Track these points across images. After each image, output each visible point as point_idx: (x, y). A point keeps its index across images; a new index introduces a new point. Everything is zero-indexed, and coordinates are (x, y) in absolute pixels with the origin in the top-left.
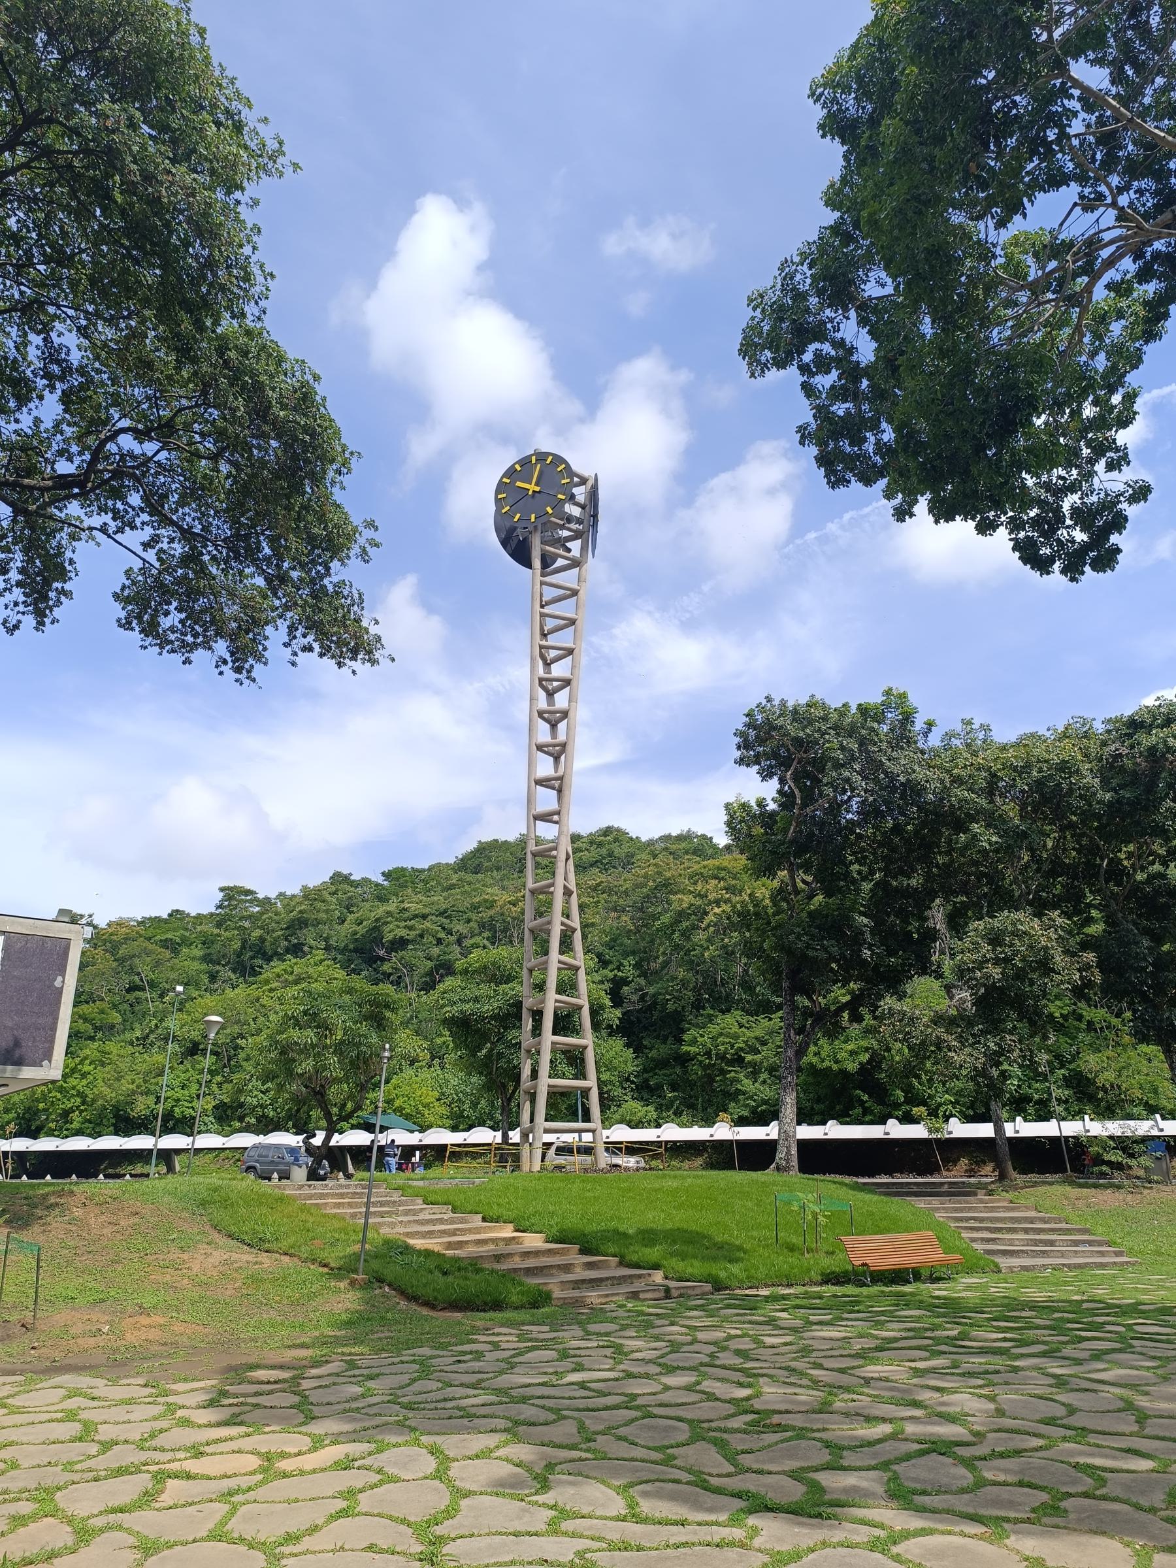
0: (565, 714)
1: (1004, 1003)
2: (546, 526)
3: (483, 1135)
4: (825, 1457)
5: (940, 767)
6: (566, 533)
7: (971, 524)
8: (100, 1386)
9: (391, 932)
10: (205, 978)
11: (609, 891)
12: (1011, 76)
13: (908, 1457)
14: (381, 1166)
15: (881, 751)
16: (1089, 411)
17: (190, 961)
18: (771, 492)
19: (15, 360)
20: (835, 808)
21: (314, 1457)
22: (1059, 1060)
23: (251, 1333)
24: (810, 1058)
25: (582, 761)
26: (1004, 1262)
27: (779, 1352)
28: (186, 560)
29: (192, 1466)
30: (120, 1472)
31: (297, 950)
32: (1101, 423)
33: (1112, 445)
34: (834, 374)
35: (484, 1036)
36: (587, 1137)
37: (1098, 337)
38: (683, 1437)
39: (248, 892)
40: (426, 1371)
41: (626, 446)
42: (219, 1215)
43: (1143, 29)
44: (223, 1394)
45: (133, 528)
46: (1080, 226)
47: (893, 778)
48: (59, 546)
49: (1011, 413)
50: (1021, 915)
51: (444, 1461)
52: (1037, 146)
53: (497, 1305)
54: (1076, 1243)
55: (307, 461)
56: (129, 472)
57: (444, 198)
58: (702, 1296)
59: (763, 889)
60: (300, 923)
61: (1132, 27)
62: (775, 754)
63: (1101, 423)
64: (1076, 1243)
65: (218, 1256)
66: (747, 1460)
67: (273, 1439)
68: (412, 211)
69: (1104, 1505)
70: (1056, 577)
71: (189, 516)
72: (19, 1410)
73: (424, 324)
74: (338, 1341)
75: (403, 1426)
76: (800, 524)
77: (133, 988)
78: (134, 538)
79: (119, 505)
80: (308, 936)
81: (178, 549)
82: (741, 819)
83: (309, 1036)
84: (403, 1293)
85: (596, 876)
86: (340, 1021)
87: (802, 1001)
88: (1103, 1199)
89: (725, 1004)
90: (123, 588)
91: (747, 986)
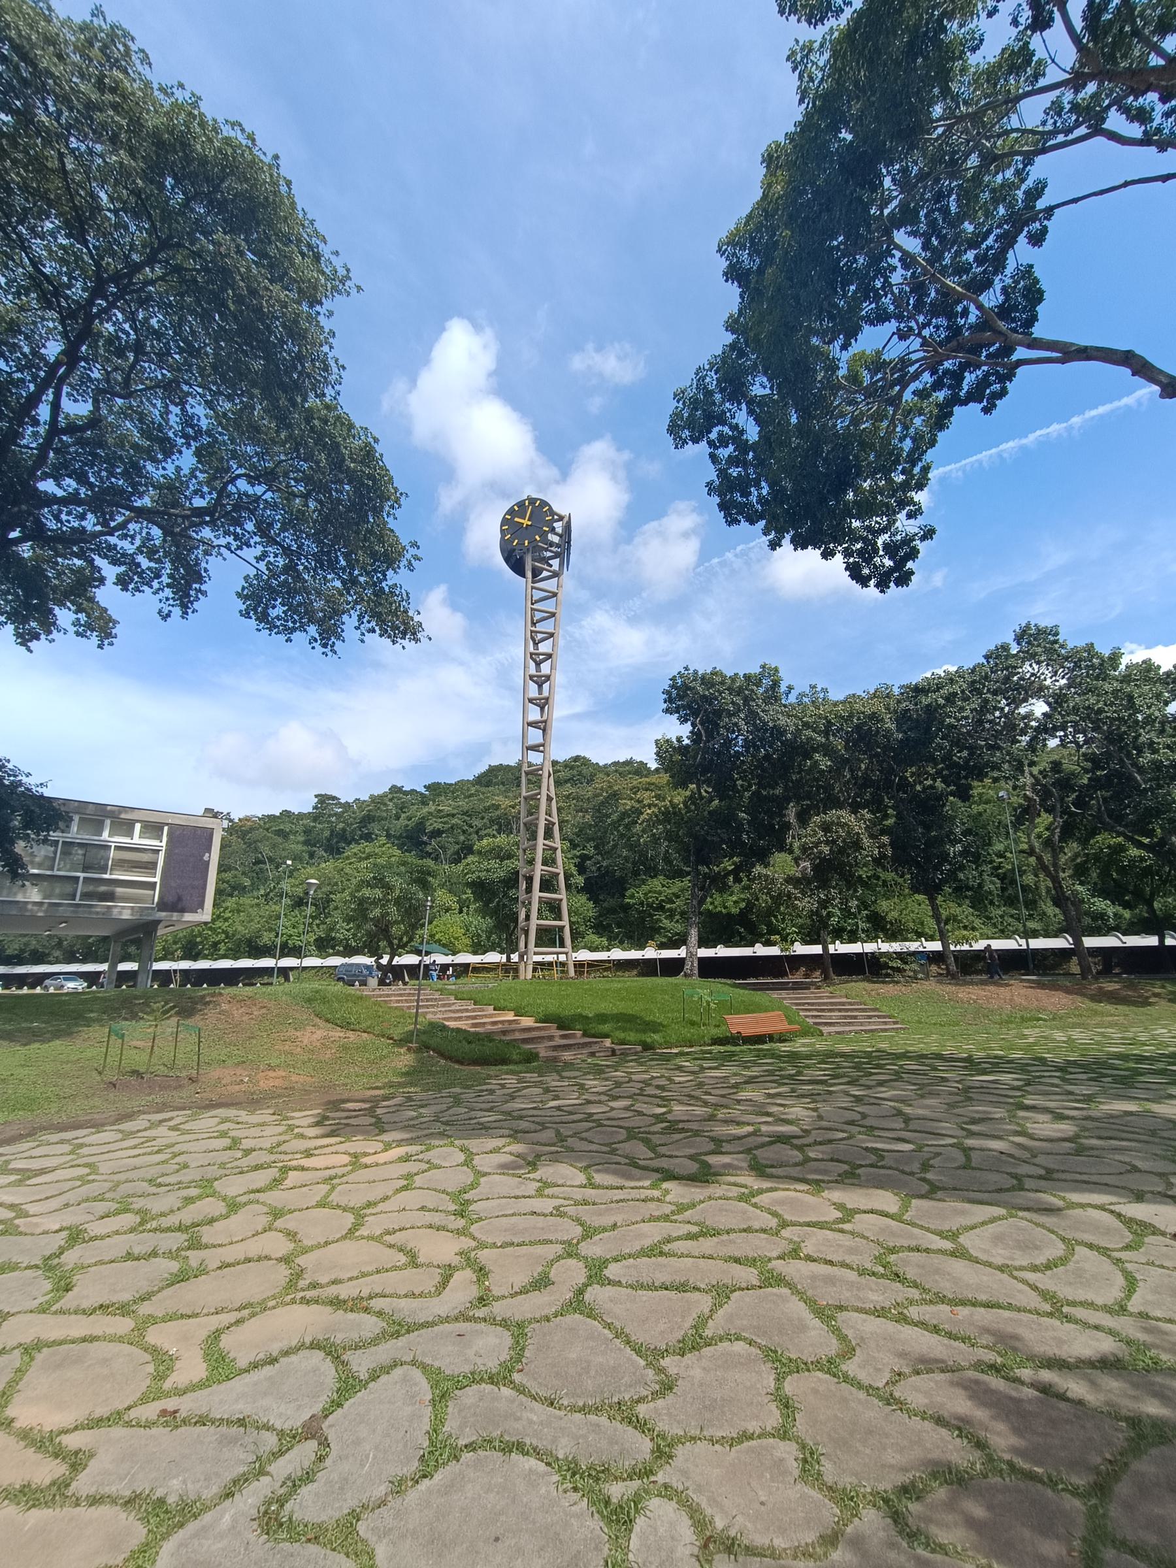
0: (548, 678)
1: (831, 870)
2: (535, 549)
3: (493, 957)
4: (712, 1146)
5: (796, 716)
6: (549, 554)
7: (818, 552)
8: (243, 1115)
9: (433, 825)
10: (306, 856)
11: (577, 798)
12: (855, 243)
13: (763, 1145)
14: (427, 976)
15: (758, 705)
16: (899, 478)
17: (296, 845)
18: (686, 535)
19: (160, 425)
20: (728, 743)
21: (385, 1155)
22: (864, 905)
23: (343, 1080)
24: (708, 906)
25: (559, 711)
26: (825, 1029)
27: (681, 1084)
28: (287, 569)
29: (306, 1162)
30: (257, 1168)
31: (368, 837)
32: (906, 486)
33: (911, 502)
34: (731, 448)
35: (494, 894)
36: (562, 958)
37: (906, 427)
38: (622, 1138)
39: (334, 798)
40: (457, 1101)
41: (588, 500)
42: (319, 1007)
43: (945, 211)
44: (327, 1118)
45: (249, 546)
46: (895, 351)
47: (765, 724)
48: (197, 559)
49: (844, 478)
50: (842, 813)
51: (470, 1156)
52: (867, 292)
53: (504, 1061)
54: (870, 1017)
55: (370, 499)
56: (249, 505)
57: (466, 322)
58: (636, 1053)
59: (679, 797)
60: (368, 819)
61: (939, 210)
62: (689, 707)
63: (906, 486)
64: (870, 1017)
65: (320, 1034)
66: (663, 1150)
67: (358, 1144)
68: (443, 329)
69: (882, 1171)
70: (872, 591)
71: (288, 538)
72: (188, 1132)
73: (453, 412)
74: (400, 1085)
75: (442, 1135)
76: (704, 555)
77: (258, 862)
78: (250, 553)
79: (238, 530)
80: (375, 828)
81: (281, 562)
82: (665, 750)
83: (378, 893)
84: (442, 1055)
85: (569, 789)
86: (398, 883)
87: (704, 869)
88: (887, 989)
89: (653, 872)
90: (243, 588)
91: (668, 860)
